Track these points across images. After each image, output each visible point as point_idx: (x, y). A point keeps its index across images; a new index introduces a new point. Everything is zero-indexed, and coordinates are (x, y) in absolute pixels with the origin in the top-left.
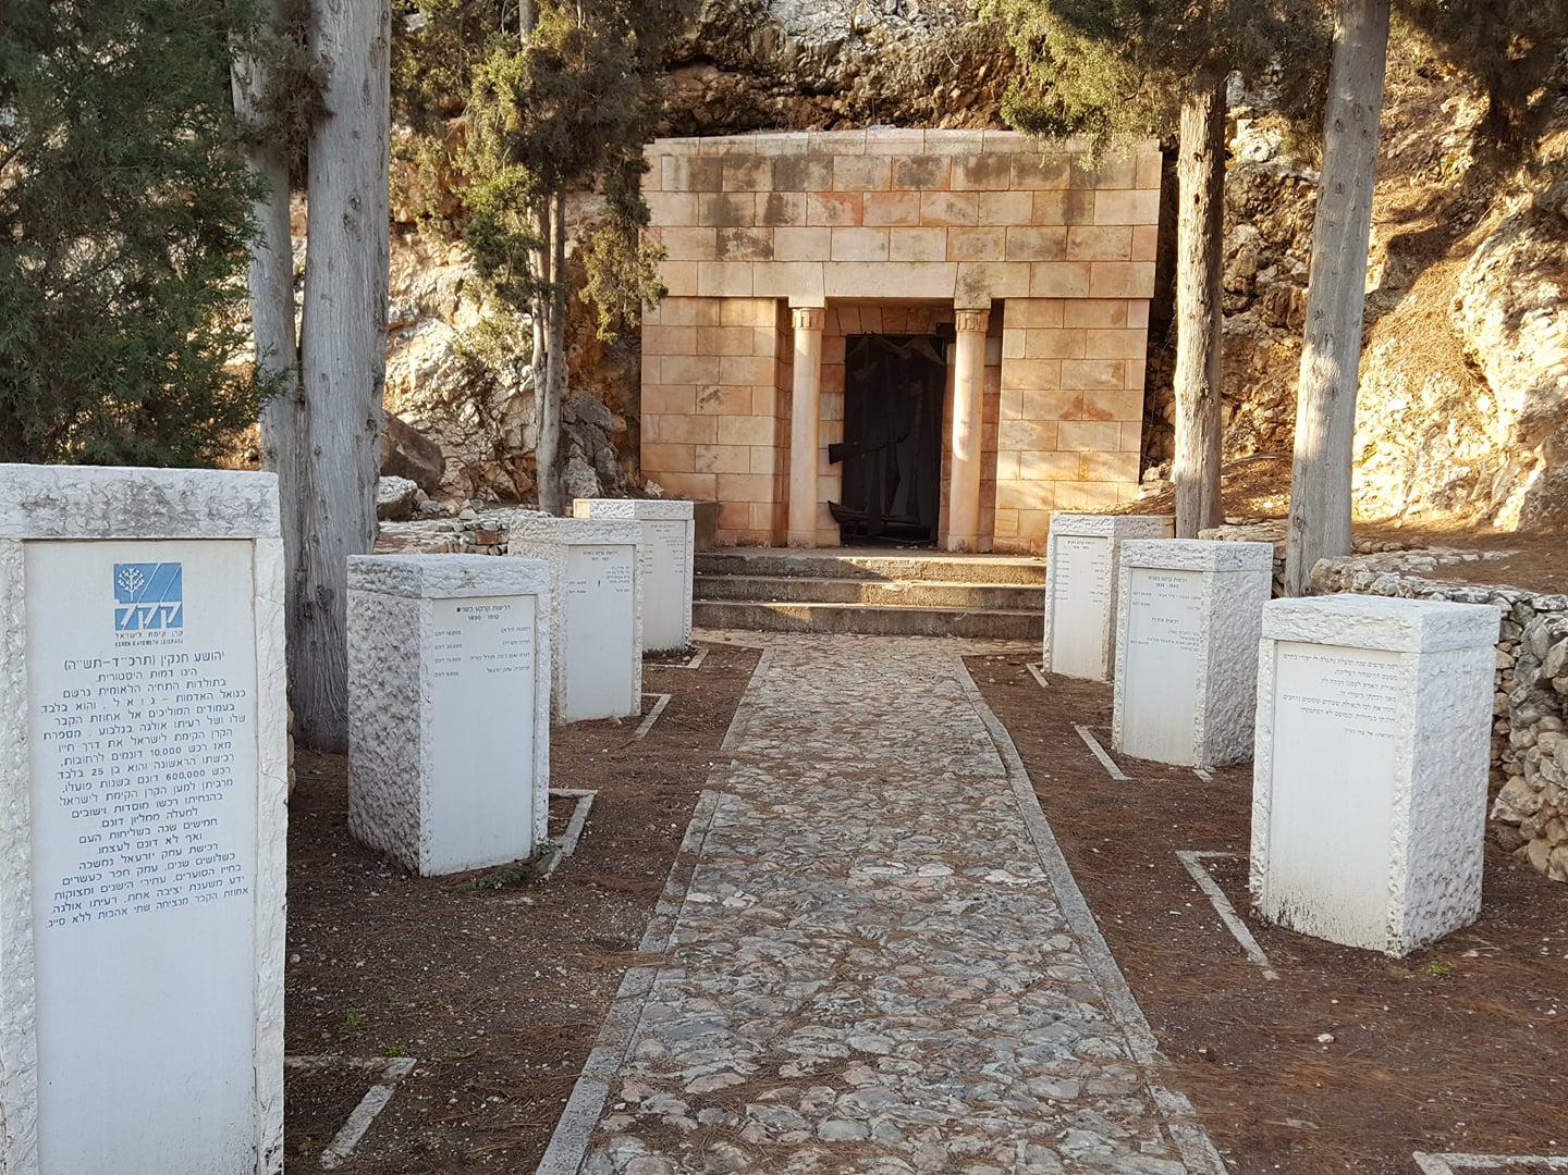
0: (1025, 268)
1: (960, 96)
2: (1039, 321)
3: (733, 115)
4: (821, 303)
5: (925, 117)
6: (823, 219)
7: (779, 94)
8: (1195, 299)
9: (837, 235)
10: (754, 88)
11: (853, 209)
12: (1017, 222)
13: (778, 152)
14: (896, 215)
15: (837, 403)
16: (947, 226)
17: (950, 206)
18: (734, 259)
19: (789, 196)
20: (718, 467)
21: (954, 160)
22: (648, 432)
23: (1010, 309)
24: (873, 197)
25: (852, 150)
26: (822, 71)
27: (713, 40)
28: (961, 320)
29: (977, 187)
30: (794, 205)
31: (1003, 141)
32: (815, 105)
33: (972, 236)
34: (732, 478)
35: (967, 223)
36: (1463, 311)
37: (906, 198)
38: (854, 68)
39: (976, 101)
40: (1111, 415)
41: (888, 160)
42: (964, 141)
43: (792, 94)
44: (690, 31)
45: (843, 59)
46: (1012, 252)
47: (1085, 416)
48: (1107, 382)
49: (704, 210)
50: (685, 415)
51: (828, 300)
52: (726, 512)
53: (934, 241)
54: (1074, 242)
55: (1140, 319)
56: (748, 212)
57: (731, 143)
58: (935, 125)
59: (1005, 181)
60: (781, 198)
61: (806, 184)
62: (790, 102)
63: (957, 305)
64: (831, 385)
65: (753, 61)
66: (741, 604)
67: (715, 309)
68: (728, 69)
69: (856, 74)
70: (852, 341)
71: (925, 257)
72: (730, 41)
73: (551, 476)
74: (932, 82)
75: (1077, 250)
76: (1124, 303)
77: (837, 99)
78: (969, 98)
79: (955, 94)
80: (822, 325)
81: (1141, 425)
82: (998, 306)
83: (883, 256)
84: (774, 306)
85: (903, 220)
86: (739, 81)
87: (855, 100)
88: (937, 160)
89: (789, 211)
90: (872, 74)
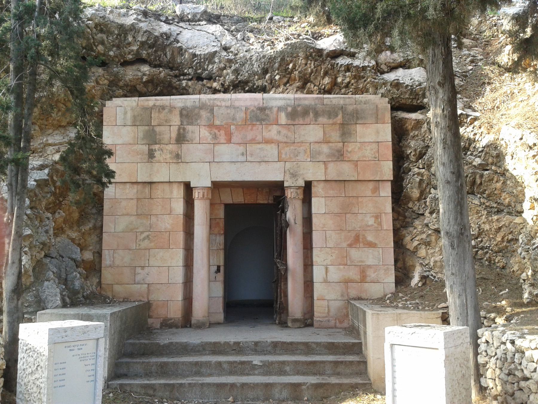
0: (322, 166)
1: (280, 78)
2: (331, 193)
3: (159, 89)
4: (209, 185)
5: (264, 90)
6: (209, 140)
7: (184, 80)
8: (449, 171)
9: (217, 148)
10: (170, 76)
11: (226, 134)
12: (316, 141)
13: (183, 105)
14: (249, 137)
15: (220, 239)
16: (278, 143)
17: (279, 132)
18: (159, 162)
19: (190, 128)
20: (149, 280)
21: (280, 109)
22: (107, 259)
23: (314, 186)
24: (236, 127)
25: (223, 104)
26: (206, 67)
27: (146, 51)
28: (289, 194)
29: (293, 123)
30: (192, 132)
31: (305, 99)
32: (204, 85)
33: (292, 148)
34: (158, 286)
35: (288, 141)
36: (64, 256)
37: (254, 128)
38: (223, 65)
39: (288, 82)
40: (376, 244)
41: (244, 109)
42: (284, 99)
43: (190, 80)
44: (133, 45)
45: (217, 61)
46: (314, 156)
47: (361, 245)
48: (372, 225)
49: (141, 135)
50: (130, 249)
51: (213, 183)
52: (154, 307)
53: (271, 151)
54: (347, 151)
55: (386, 191)
56: (166, 137)
57: (156, 100)
58: (268, 92)
59: (308, 120)
60: (184, 129)
61: (199, 121)
62: (190, 83)
63: (286, 184)
64: (216, 230)
65: (169, 62)
66: (153, 382)
67: (147, 190)
68: (155, 66)
69: (225, 68)
70: (227, 206)
71: (266, 159)
72: (156, 51)
73: (10, 300)
74: (265, 71)
75: (349, 155)
76: (378, 182)
77: (215, 82)
78: (285, 80)
79: (277, 77)
80: (210, 196)
81: (393, 250)
82: (308, 186)
83: (243, 159)
84: (182, 187)
85: (253, 140)
86: (163, 73)
87: (224, 81)
88: (271, 109)
89: (189, 136)
90: (233, 68)
